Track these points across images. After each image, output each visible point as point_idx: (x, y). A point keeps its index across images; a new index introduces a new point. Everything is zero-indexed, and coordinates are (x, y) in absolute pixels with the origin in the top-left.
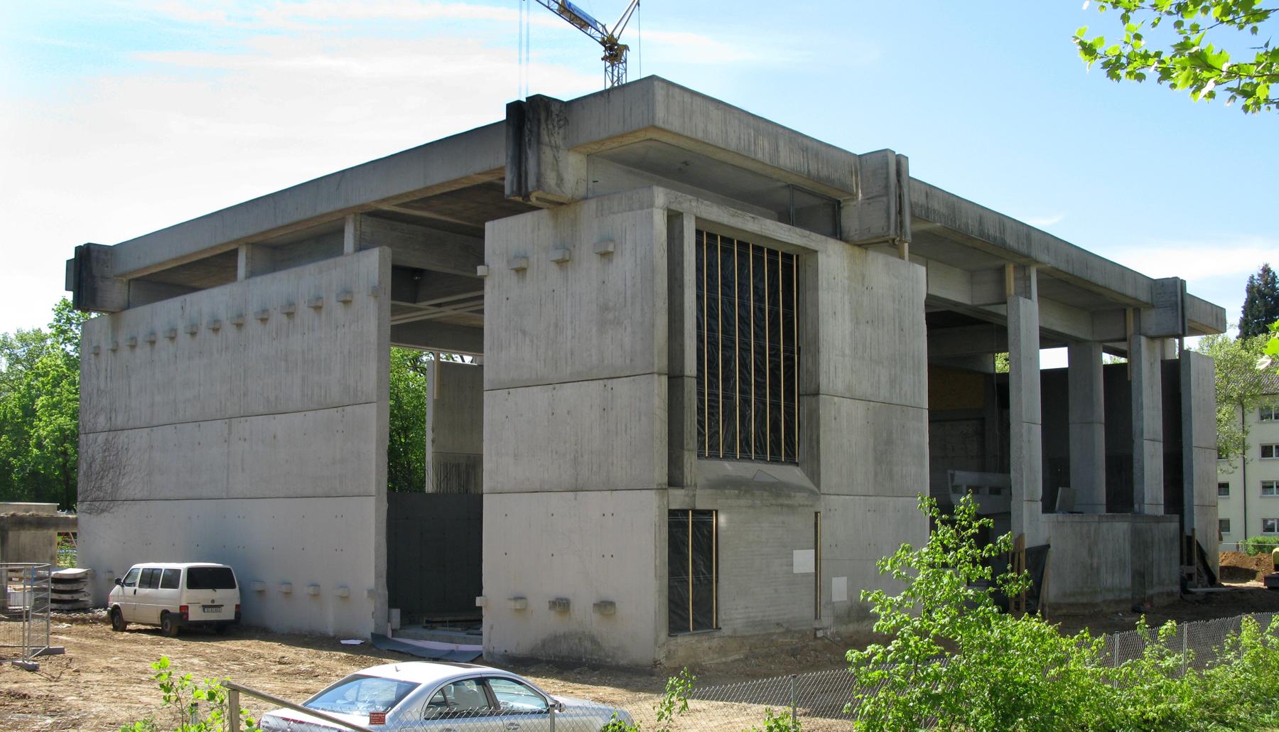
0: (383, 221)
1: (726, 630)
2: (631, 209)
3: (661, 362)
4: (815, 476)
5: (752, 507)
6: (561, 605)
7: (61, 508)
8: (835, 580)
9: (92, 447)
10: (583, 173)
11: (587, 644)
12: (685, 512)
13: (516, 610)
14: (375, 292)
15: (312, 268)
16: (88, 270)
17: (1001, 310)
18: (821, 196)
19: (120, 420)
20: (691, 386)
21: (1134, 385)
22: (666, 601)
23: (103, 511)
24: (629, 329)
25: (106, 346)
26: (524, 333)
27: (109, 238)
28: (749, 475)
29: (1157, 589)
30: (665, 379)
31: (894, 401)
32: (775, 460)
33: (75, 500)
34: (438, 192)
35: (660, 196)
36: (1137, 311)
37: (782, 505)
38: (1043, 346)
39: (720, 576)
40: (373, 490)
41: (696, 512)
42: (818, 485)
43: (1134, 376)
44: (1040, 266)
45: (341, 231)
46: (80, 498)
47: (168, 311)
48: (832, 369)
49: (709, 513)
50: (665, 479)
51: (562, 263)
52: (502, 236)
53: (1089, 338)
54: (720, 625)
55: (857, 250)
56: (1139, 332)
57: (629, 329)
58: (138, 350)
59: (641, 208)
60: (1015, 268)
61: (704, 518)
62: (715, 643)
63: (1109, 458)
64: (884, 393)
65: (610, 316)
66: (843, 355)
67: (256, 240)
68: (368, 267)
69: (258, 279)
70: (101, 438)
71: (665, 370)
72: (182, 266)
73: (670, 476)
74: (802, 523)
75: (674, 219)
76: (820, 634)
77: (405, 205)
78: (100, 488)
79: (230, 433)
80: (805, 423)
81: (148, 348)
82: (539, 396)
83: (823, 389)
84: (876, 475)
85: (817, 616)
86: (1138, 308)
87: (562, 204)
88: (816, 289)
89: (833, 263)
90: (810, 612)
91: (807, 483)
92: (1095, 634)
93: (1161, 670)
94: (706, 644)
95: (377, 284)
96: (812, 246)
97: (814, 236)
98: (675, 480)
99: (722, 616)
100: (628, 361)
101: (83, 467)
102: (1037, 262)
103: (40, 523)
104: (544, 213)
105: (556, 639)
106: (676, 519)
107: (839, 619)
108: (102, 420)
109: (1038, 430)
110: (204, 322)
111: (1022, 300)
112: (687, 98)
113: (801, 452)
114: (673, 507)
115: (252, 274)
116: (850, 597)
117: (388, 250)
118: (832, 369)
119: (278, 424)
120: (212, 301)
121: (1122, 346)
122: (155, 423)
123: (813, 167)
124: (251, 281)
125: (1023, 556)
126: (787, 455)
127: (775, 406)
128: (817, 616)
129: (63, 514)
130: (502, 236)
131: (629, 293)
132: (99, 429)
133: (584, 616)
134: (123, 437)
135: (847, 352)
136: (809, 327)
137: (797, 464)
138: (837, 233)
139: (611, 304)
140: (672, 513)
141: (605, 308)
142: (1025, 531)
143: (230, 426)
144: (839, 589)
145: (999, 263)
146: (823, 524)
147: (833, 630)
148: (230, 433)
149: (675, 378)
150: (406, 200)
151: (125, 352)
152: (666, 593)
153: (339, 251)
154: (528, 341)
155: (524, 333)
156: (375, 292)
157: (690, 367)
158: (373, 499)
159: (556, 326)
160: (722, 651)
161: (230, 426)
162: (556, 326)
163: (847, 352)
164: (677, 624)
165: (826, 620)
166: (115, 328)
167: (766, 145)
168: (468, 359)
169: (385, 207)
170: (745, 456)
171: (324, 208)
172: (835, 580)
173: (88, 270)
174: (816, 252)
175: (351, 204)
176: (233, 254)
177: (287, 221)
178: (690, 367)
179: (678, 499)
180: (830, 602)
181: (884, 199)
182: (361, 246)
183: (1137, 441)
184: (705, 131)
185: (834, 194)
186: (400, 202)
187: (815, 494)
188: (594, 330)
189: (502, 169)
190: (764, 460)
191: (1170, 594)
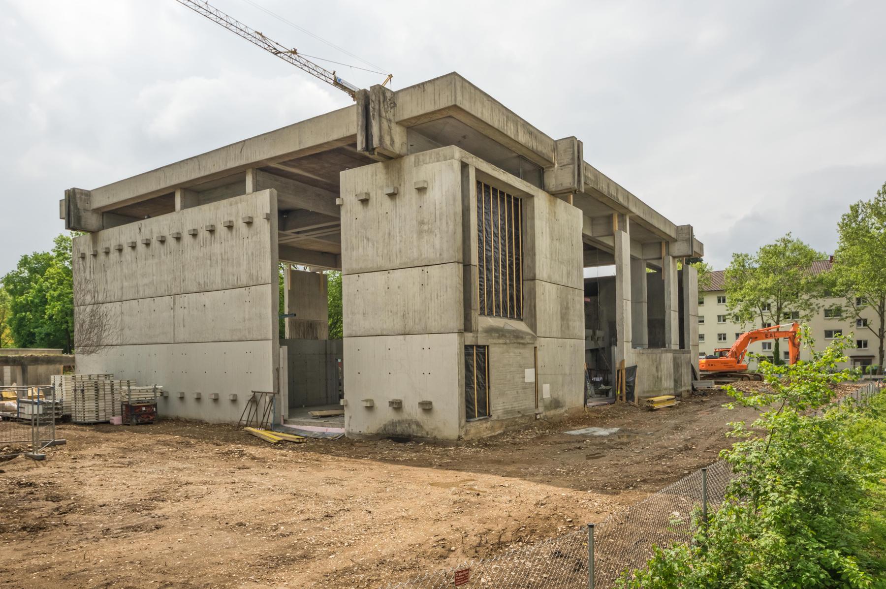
0: (268, 172)
1: (494, 417)
2: (438, 161)
3: (460, 256)
4: (533, 326)
5: (505, 344)
6: (397, 406)
7: (63, 352)
8: (544, 386)
9: (82, 314)
10: (405, 139)
11: (414, 427)
12: (472, 347)
13: (367, 407)
14: (268, 218)
15: (225, 202)
16: (75, 208)
17: (608, 241)
18: (534, 164)
19: (101, 298)
20: (475, 272)
21: (666, 282)
22: (464, 400)
23: (91, 352)
24: (438, 236)
25: (89, 253)
26: (368, 239)
27: (88, 185)
28: (502, 325)
29: (683, 389)
30: (461, 266)
32: (512, 317)
33: (73, 347)
34: (308, 154)
35: (457, 152)
36: (667, 243)
37: (519, 343)
38: (585, 266)
39: (491, 385)
40: (270, 337)
41: (478, 347)
42: (535, 332)
43: (666, 277)
44: (631, 215)
45: (243, 181)
46: (76, 345)
47: (126, 233)
49: (484, 347)
50: (462, 327)
51: (392, 196)
52: (354, 181)
53: (640, 257)
54: (491, 413)
55: (552, 197)
56: (668, 254)
57: (438, 236)
58: (111, 255)
59: (445, 159)
60: (618, 216)
61: (483, 351)
62: (489, 424)
63: (649, 321)
64: (564, 281)
65: (426, 227)
67: (187, 186)
68: (260, 202)
69: (190, 210)
70: (89, 309)
71: (461, 260)
72: (139, 204)
73: (465, 324)
74: (528, 353)
75: (464, 166)
76: (538, 417)
77: (284, 163)
78: (89, 339)
79: (174, 304)
80: (526, 297)
81: (117, 254)
82: (379, 278)
83: (537, 277)
85: (537, 407)
86: (669, 241)
87: (391, 158)
88: (533, 218)
89: (541, 201)
90: (533, 405)
91: (528, 330)
94: (485, 425)
95: (268, 212)
96: (532, 192)
98: (467, 326)
99: (492, 408)
100: (438, 255)
101: (77, 327)
102: (631, 212)
103: (49, 361)
104: (380, 165)
105: (394, 424)
106: (468, 349)
107: (547, 408)
108: (88, 298)
109: (629, 303)
110: (155, 238)
111: (623, 233)
112: (473, 90)
113: (525, 313)
114: (467, 343)
115: (184, 207)
116: (551, 395)
117: (275, 191)
119: (206, 298)
120: (159, 225)
121: (655, 263)
122: (124, 298)
124: (185, 211)
125: (624, 372)
127: (511, 286)
128: (537, 407)
129: (64, 355)
130: (354, 181)
131: (438, 212)
132: (87, 302)
133: (412, 410)
134: (103, 308)
136: (529, 240)
137: (522, 320)
138: (542, 185)
139: (426, 221)
140: (466, 347)
141: (422, 223)
143: (174, 300)
144: (546, 391)
145: (610, 212)
146: (539, 354)
147: (544, 414)
148: (174, 304)
149: (466, 266)
150: (287, 159)
151: (102, 257)
152: (464, 395)
154: (370, 244)
155: (368, 239)
156: (268, 218)
157: (475, 260)
158: (270, 342)
159: (389, 234)
160: (492, 428)
161: (174, 300)
162: (389, 234)
164: (469, 415)
165: (541, 409)
166: (95, 241)
168: (301, 268)
169: (273, 165)
170: (498, 315)
171: (232, 164)
172: (544, 386)
173: (75, 208)
174: (533, 196)
175: (250, 162)
176: (172, 195)
177: (207, 173)
178: (475, 260)
179: (469, 338)
180: (542, 399)
181: (571, 166)
182: (257, 188)
183: (667, 311)
185: (542, 163)
186: (282, 161)
187: (534, 338)
188: (415, 236)
189: (355, 136)
191: (688, 391)
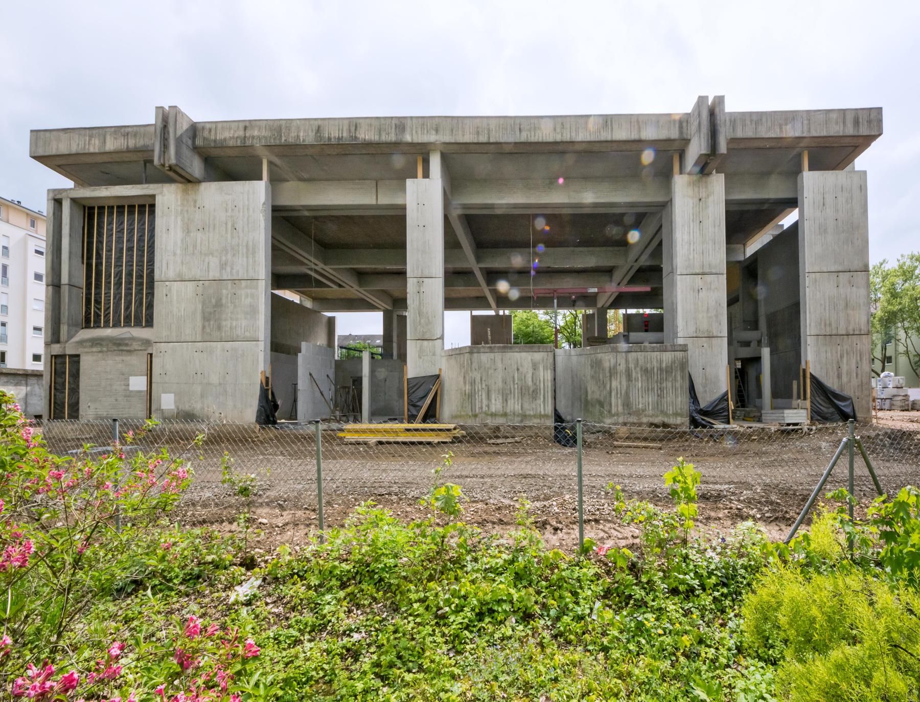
31: (225, 277)
48: (164, 265)
64: (214, 274)
66: (175, 254)
74: (139, 361)
84: (204, 328)
92: (895, 323)
93: (626, 617)
97: (152, 186)
118: (164, 265)
123: (132, 143)
126: (147, 321)
135: (178, 252)
142: (443, 368)
149: (55, 285)
153: (406, 317)
163: (178, 252)
167: (97, 142)
184: (57, 149)
190: (130, 326)
